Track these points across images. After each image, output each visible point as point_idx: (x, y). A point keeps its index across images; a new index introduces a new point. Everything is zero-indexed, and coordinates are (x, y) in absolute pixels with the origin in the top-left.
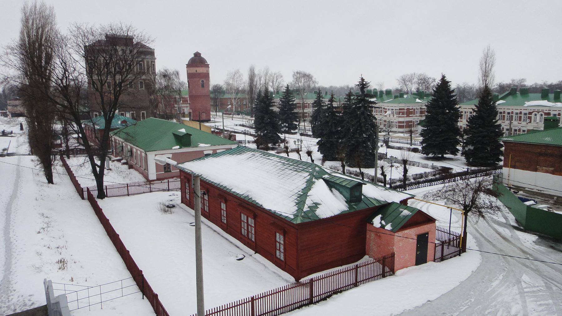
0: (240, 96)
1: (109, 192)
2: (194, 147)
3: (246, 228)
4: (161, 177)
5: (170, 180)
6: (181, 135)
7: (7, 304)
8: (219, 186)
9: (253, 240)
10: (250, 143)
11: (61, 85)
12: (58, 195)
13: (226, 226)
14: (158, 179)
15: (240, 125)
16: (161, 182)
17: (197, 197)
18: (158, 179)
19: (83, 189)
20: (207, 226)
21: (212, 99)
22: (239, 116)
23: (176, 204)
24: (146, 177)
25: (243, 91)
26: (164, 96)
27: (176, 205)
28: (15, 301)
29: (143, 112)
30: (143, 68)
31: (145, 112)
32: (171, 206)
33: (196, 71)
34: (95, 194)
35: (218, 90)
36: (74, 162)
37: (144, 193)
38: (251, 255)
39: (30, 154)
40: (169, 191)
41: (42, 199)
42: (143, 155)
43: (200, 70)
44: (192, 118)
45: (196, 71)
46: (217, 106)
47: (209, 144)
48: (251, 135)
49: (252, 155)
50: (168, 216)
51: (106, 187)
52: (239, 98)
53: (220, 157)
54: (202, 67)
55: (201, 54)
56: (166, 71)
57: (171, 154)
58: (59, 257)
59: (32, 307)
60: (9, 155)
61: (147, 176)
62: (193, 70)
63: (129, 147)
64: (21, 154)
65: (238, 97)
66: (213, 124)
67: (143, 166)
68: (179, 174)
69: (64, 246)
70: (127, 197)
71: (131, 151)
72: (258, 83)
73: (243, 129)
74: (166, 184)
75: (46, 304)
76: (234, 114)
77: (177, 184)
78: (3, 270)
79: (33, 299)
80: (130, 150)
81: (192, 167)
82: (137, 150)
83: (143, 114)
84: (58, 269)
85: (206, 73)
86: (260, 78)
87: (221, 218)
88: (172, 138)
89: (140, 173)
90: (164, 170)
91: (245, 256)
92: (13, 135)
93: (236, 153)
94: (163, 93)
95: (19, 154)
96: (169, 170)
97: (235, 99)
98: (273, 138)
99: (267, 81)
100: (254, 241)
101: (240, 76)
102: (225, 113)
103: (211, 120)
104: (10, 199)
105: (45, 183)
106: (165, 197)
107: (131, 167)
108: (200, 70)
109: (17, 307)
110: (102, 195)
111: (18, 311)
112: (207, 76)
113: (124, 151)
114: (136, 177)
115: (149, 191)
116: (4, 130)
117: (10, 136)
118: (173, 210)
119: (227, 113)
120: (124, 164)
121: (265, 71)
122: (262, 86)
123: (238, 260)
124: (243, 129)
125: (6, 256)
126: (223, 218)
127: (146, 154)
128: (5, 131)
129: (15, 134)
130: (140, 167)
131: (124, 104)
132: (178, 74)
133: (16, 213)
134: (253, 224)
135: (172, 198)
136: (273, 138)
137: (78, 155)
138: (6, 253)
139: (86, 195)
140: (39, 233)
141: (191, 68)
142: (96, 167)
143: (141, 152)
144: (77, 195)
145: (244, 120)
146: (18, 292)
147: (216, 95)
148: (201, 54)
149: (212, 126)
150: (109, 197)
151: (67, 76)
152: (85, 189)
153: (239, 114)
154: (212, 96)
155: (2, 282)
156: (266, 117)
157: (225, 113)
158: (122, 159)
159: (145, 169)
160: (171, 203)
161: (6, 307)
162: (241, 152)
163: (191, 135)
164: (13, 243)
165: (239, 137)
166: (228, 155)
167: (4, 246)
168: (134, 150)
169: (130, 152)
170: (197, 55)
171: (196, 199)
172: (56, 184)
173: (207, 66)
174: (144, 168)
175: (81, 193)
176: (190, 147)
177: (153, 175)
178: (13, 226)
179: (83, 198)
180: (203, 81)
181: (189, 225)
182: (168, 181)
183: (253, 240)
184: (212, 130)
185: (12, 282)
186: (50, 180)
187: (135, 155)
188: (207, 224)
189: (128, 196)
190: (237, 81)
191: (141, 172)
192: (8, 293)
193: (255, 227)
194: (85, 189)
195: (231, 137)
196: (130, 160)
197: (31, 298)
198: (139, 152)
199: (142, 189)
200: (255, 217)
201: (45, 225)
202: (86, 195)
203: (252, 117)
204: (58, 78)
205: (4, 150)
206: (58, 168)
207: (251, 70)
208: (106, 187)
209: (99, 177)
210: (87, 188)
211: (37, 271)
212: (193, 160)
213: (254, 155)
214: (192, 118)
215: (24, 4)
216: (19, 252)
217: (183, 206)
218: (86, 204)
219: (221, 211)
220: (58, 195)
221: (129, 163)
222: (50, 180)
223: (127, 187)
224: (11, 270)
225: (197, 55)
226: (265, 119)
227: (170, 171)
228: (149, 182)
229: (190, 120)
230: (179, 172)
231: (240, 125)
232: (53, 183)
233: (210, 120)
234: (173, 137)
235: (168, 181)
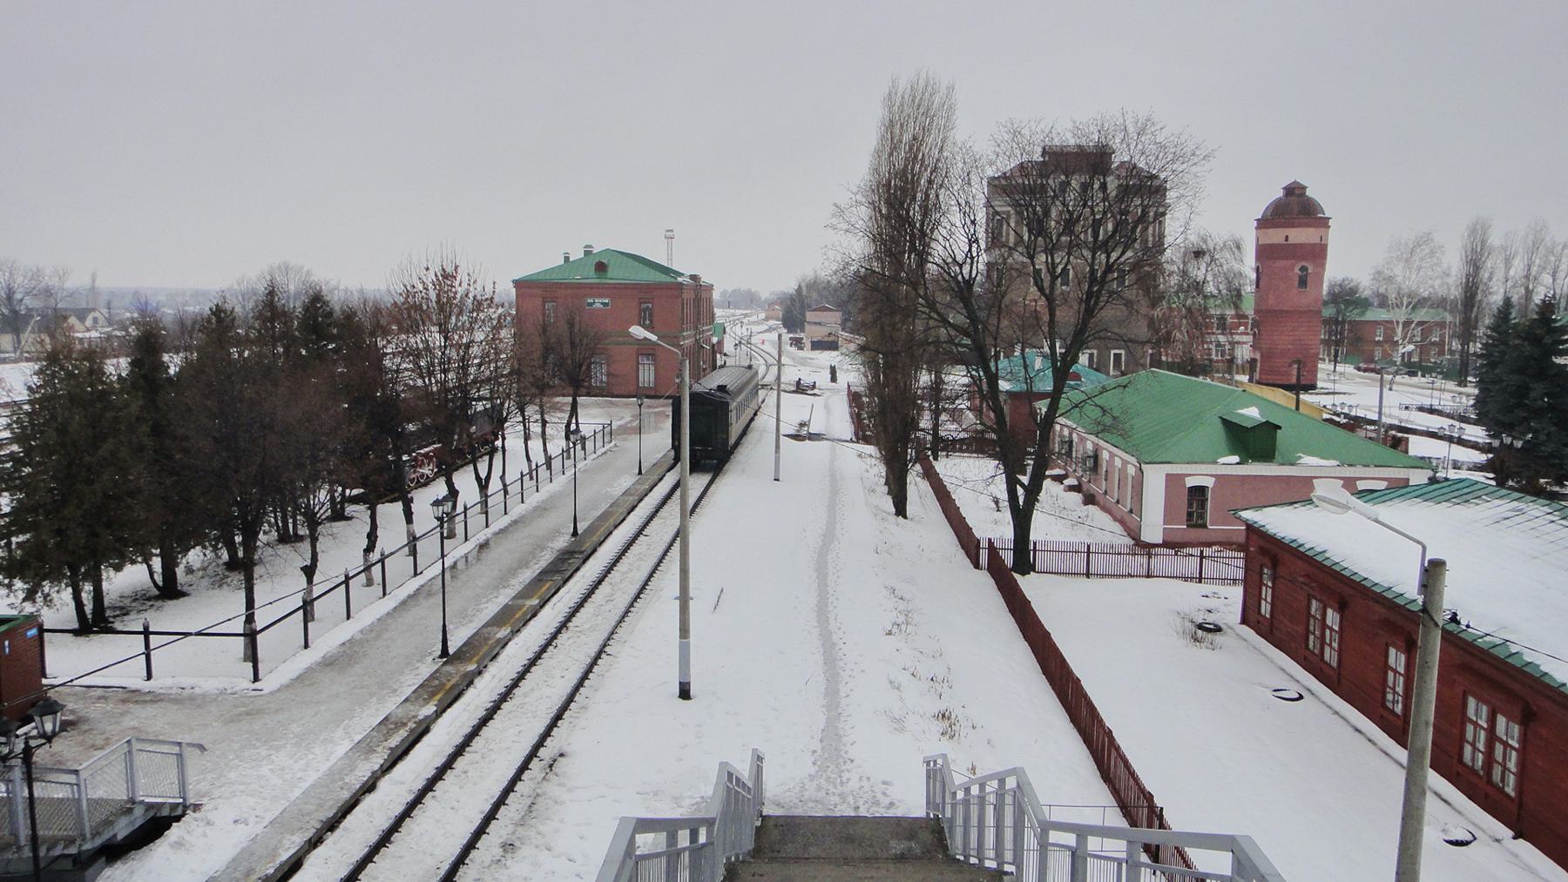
0: (1422, 315)
1: (1041, 560)
2: (1283, 465)
3: (1481, 746)
4: (1178, 539)
5: (1207, 551)
6: (1249, 425)
7: (840, 789)
8: (1389, 595)
9: (1510, 790)
10: (1459, 469)
11: (960, 277)
12: (919, 546)
13: (1400, 723)
14: (1166, 544)
15: (1421, 409)
16: (1176, 554)
17: (1432, 624)
18: (1165, 544)
19: (979, 541)
20: (1330, 708)
21: (1327, 322)
22: (1415, 380)
23: (1225, 624)
24: (1134, 534)
25: (1441, 303)
26: (1189, 310)
27: (1223, 626)
28: (854, 784)
29: (1117, 351)
30: (1004, 234)
31: (1123, 352)
32: (1212, 627)
33: (1287, 237)
34: (1008, 558)
35: (1346, 297)
36: (949, 467)
37: (1130, 576)
38: (1498, 841)
39: (854, 439)
40: (1200, 582)
41: (887, 552)
42: (1131, 470)
43: (1301, 235)
44: (1257, 376)
45: (1287, 237)
46: (1338, 343)
47: (1334, 458)
48: (1475, 446)
49: (1514, 510)
50: (1200, 654)
51: (1035, 544)
52: (1420, 323)
53: (1389, 503)
54: (1308, 225)
55: (1304, 188)
56: (1241, 239)
57: (1212, 476)
58: (941, 706)
59: (891, 813)
60: (812, 437)
61: (1138, 532)
62: (1276, 236)
63: (1089, 446)
64: (836, 437)
65: (1416, 320)
66: (1326, 401)
67: (1126, 500)
68: (1242, 539)
69: (946, 680)
70: (1084, 579)
71: (1096, 457)
72: (1499, 275)
73: (1435, 423)
74: (1195, 561)
75: (1075, 835)
76: (1396, 373)
77: (1234, 565)
78: (823, 706)
79: (895, 793)
80: (1091, 454)
81: (1281, 522)
82: (1112, 455)
83: (1117, 356)
84: (939, 735)
85: (1315, 245)
86: (1508, 262)
87: (1384, 694)
88: (1219, 431)
89: (1115, 519)
90: (1187, 521)
91: (1475, 839)
92: (816, 391)
93: (1447, 497)
94: (1189, 302)
95: (831, 438)
96: (1200, 522)
97: (1407, 324)
98: (1557, 461)
99: (1534, 270)
100: (1513, 794)
101: (1432, 253)
102: (1362, 365)
103: (1320, 384)
104: (823, 540)
105: (888, 514)
106: (1192, 599)
107: (1090, 500)
108: (1301, 235)
109: (861, 803)
110: (1025, 563)
111: (863, 812)
112: (1318, 253)
113: (1074, 456)
114: (1103, 529)
115: (1145, 572)
116: (800, 379)
117: (811, 395)
118: (1218, 638)
119: (1372, 366)
120: (1071, 488)
121: (1531, 237)
122: (1514, 286)
123: (1447, 841)
124: (1435, 423)
125: (827, 675)
126: (1390, 697)
127: (1141, 469)
128: (802, 382)
129: (820, 389)
130: (1118, 502)
131: (1105, 330)
132: (1238, 247)
133: (838, 577)
134: (1513, 738)
135: (1211, 603)
136: (1557, 461)
137: (957, 454)
138: (826, 668)
139: (984, 557)
140: (890, 633)
141: (1271, 231)
142: (1018, 486)
143: (1125, 463)
144: (961, 555)
145: (1436, 393)
146: (859, 767)
147: (1338, 312)
148: (1304, 188)
149: (1322, 404)
150: (1038, 572)
151: (975, 254)
152: (984, 544)
153: (1412, 374)
154: (1328, 312)
155: (824, 734)
156: (1538, 388)
157: (1362, 365)
158: (1065, 476)
159: (1131, 511)
160: (1211, 618)
161: (839, 795)
162: (1467, 497)
163: (1280, 428)
164: (838, 647)
165: (1418, 446)
166: (1418, 500)
167: (821, 650)
168: (1105, 455)
169: (1092, 460)
170: (1294, 191)
171: (1427, 634)
172: (912, 519)
173: (1324, 223)
174: (1129, 508)
175: (973, 552)
176: (1272, 462)
177: (1153, 528)
178: (834, 607)
179: (977, 566)
180: (1303, 269)
181: (1270, 694)
182: (1202, 552)
183: (1510, 790)
184: (1326, 416)
185: (844, 740)
186: (901, 510)
187: (1105, 470)
188: (1329, 702)
189: (1088, 578)
190: (1419, 269)
191: (549, 471)
192: (839, 763)
193: (1523, 752)
194: (984, 544)
195: (1395, 439)
196: (1089, 481)
197: (887, 789)
198: (1118, 462)
199: (1113, 564)
200: (1527, 718)
201: (901, 619)
202: (984, 557)
203: (1463, 383)
204: (954, 259)
205: (802, 425)
206: (917, 486)
207: (1473, 231)
208: (1035, 544)
209: (1022, 519)
210: (990, 540)
211: (896, 726)
212: (1292, 503)
213: (1522, 512)
214: (1257, 376)
215: (891, 84)
216: (852, 670)
217: (1247, 632)
218: (984, 580)
219: (1386, 674)
220: (919, 546)
221: (1085, 488)
222: (901, 510)
223: (1088, 552)
224: (840, 710)
225: (1294, 191)
226: (1533, 394)
227: (1204, 526)
228: (1147, 548)
229: (1251, 380)
230: (1244, 533)
231: (1421, 409)
232: (905, 517)
233: (1313, 387)
234: (1220, 427)
235: (1202, 552)
